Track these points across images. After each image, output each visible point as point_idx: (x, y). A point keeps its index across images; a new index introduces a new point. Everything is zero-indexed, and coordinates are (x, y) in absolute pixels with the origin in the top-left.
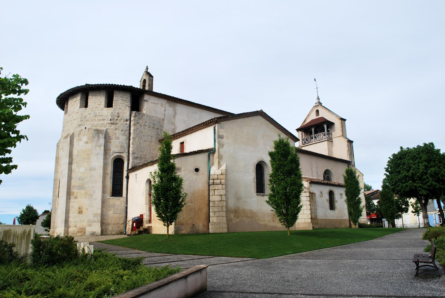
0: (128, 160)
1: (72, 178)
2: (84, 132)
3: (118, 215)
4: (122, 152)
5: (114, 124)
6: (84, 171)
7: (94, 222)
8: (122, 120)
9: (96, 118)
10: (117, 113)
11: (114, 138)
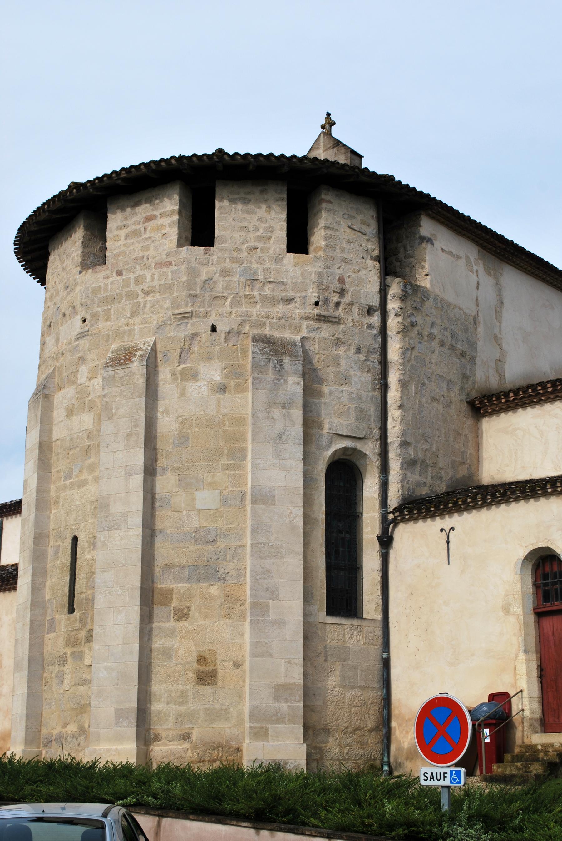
0: (384, 469)
1: (157, 533)
2: (208, 344)
3: (357, 692)
4: (362, 436)
5: (329, 322)
6: (218, 506)
7: (278, 719)
8: (356, 309)
9: (255, 293)
10: (337, 278)
11: (332, 376)
